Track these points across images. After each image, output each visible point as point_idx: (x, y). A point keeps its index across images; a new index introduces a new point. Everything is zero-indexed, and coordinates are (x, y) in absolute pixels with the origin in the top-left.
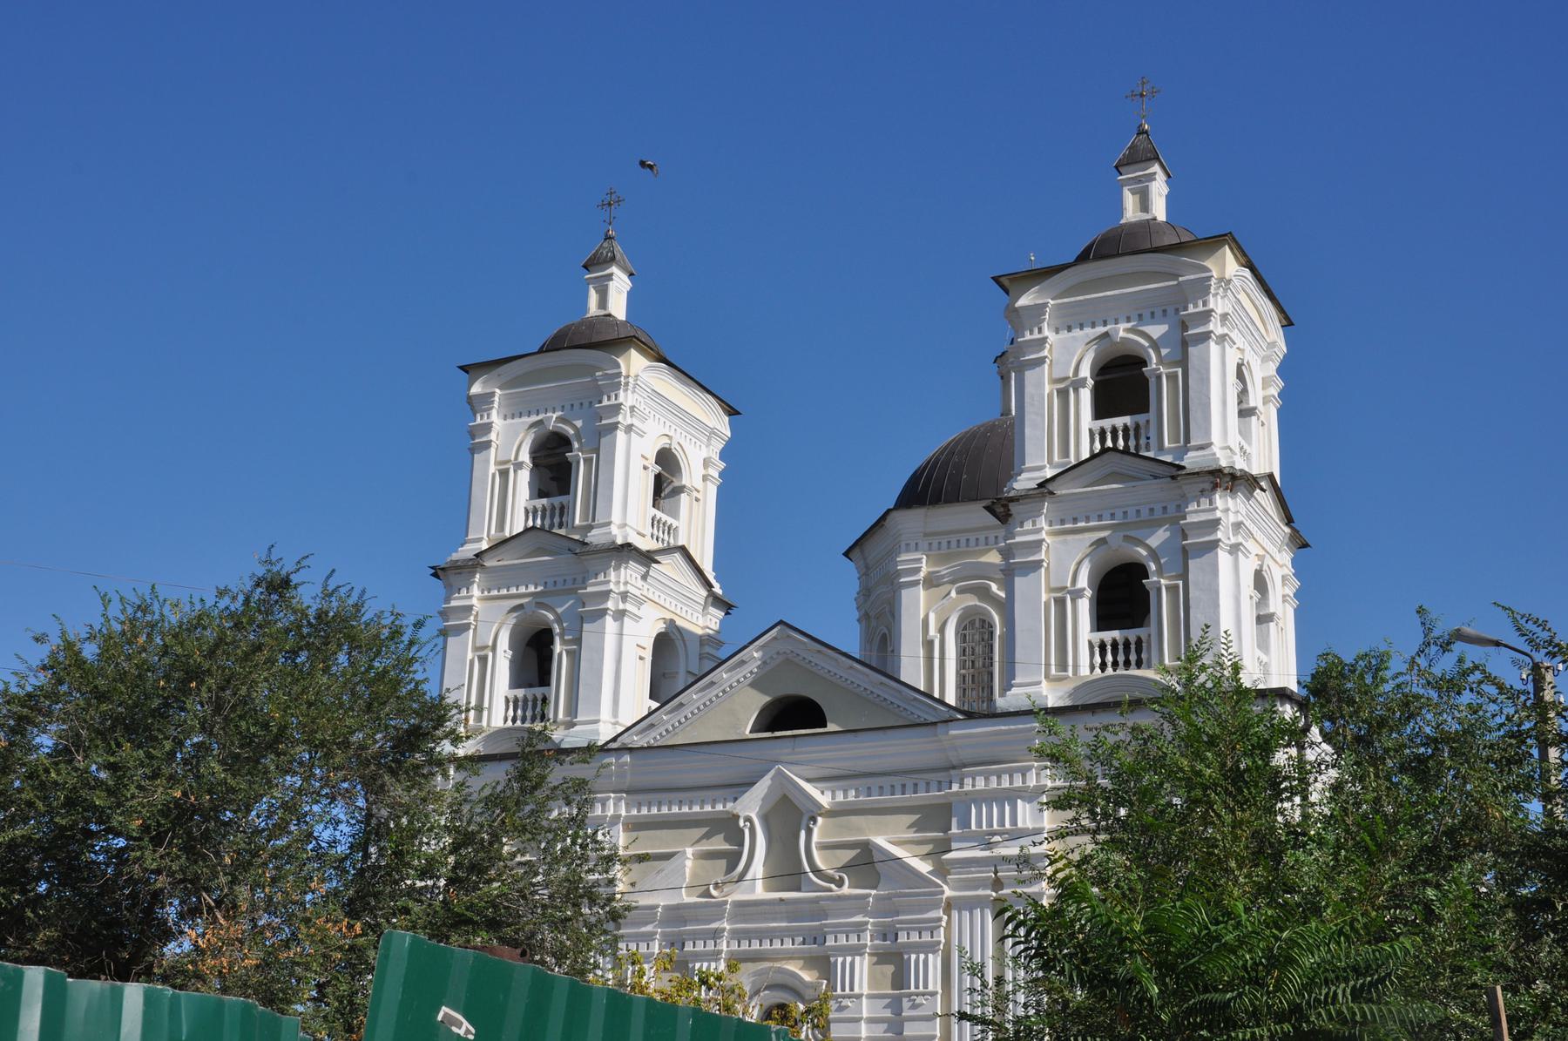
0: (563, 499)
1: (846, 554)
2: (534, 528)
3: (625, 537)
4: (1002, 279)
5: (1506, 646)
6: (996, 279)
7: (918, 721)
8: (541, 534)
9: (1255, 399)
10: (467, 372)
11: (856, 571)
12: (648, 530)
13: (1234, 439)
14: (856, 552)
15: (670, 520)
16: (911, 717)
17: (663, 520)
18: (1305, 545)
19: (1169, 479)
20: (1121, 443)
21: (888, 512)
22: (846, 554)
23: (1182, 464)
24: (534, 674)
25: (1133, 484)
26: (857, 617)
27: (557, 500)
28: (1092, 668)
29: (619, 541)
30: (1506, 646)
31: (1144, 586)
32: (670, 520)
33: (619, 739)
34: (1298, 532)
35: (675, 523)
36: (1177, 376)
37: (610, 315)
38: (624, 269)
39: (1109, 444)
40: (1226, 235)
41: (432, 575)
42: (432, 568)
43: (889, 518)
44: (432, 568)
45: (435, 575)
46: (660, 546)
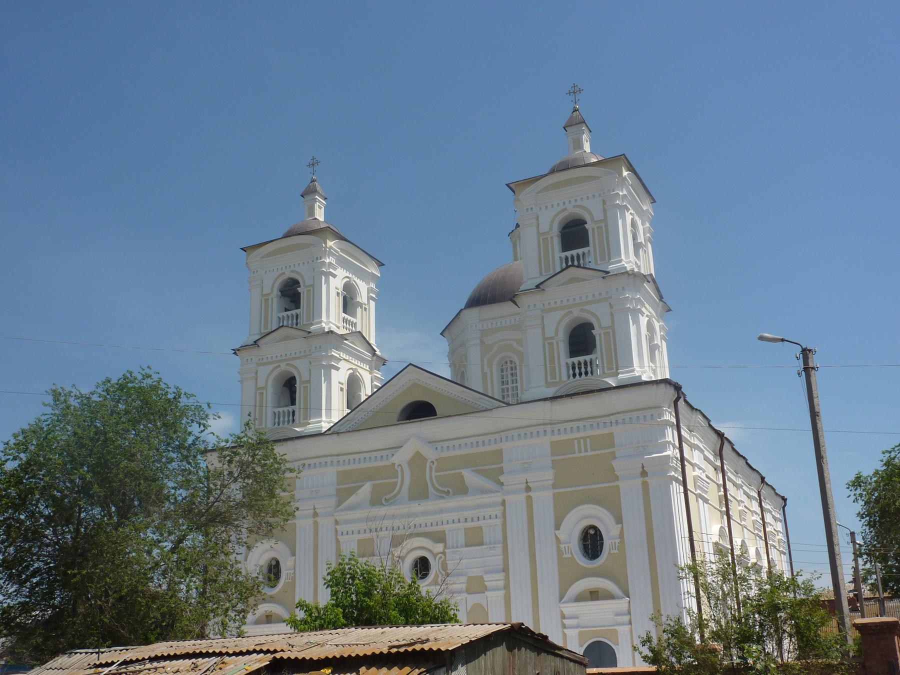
0: (298, 311)
1: (441, 334)
2: (283, 326)
3: (330, 328)
4: (511, 185)
5: (787, 341)
6: (507, 185)
7: (483, 409)
8: (287, 329)
9: (641, 239)
10: (245, 251)
11: (447, 342)
12: (341, 324)
13: (632, 257)
14: (447, 331)
15: (352, 319)
16: (480, 407)
17: (352, 320)
18: (669, 310)
19: (602, 279)
20: (576, 263)
21: (462, 310)
22: (441, 334)
23: (608, 270)
24: (288, 400)
25: (583, 282)
26: (448, 344)
27: (294, 312)
28: (569, 377)
29: (326, 330)
30: (787, 341)
31: (592, 333)
32: (352, 319)
33: (332, 429)
34: (666, 303)
35: (354, 320)
36: (602, 227)
37: (316, 219)
38: (321, 196)
39: (570, 263)
40: (621, 155)
41: (234, 353)
42: (233, 350)
43: (462, 314)
44: (233, 350)
45: (235, 353)
46: (348, 332)
